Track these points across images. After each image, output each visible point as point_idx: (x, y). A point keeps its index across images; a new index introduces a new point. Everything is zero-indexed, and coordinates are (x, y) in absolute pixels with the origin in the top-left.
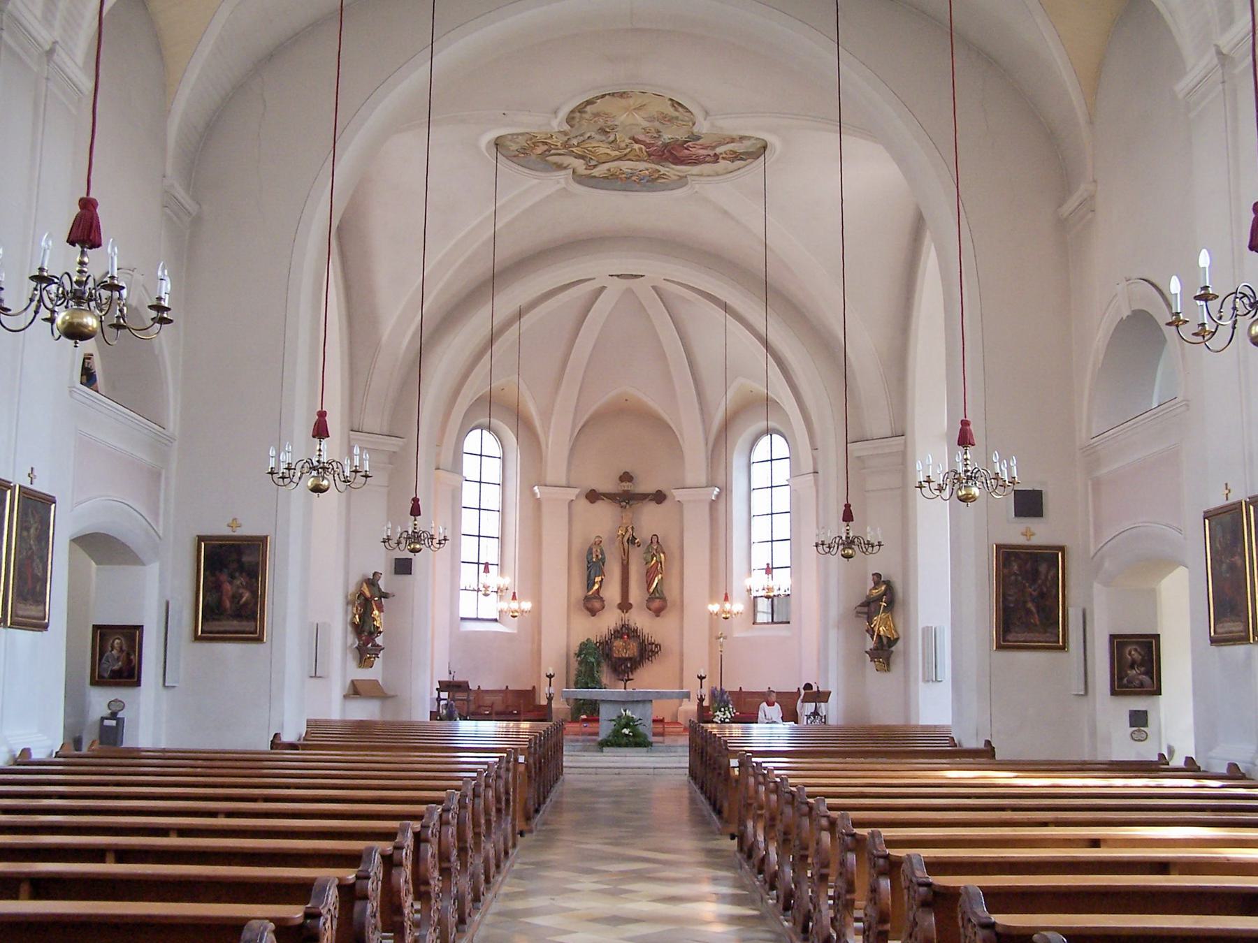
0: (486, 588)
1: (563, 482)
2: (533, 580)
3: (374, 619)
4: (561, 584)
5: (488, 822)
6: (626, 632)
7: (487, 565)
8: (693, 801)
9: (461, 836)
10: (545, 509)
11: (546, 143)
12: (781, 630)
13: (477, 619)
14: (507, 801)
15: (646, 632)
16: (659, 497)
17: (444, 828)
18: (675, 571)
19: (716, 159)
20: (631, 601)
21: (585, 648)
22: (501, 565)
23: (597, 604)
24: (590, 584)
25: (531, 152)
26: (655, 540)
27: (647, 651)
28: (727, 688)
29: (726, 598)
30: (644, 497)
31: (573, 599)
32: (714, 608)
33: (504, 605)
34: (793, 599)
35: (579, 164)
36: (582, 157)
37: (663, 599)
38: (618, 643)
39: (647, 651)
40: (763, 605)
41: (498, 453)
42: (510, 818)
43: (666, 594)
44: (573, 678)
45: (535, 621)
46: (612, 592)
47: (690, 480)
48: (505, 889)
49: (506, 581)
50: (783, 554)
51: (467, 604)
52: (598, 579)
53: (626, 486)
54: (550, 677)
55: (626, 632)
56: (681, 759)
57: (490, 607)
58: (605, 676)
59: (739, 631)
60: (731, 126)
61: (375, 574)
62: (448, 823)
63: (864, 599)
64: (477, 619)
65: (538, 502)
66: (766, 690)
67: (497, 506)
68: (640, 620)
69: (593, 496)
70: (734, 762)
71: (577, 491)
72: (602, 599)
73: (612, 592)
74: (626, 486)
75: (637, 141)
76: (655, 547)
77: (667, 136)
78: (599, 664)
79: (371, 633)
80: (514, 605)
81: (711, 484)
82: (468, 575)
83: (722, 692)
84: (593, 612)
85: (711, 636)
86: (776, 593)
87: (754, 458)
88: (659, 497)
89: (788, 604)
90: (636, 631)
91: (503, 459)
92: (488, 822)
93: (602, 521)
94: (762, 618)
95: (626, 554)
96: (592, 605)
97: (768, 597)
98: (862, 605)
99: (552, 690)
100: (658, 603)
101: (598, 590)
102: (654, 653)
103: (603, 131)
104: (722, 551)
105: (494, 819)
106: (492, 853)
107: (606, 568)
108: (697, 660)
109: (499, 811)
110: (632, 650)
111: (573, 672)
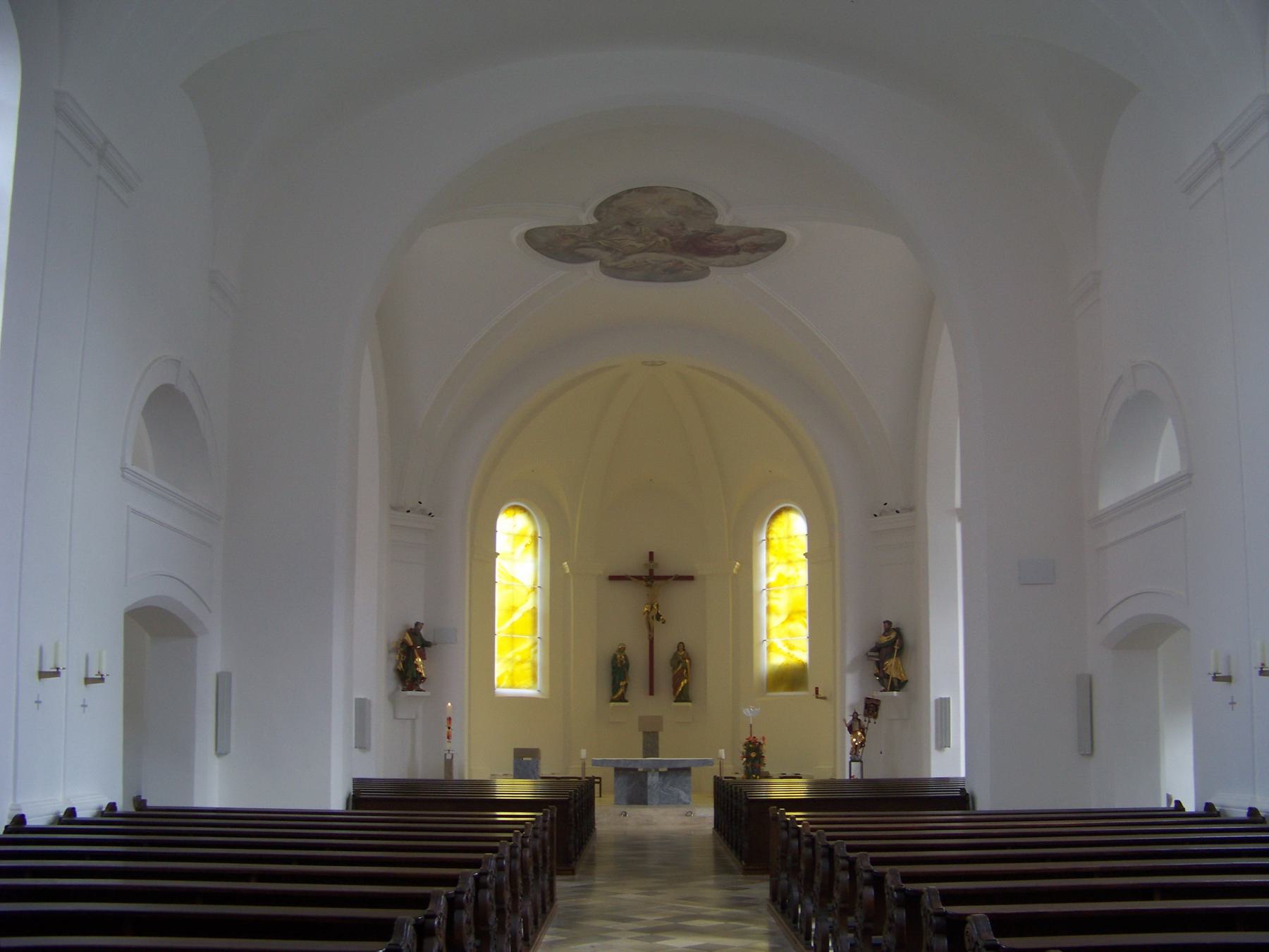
3: (416, 666)
5: (525, 882)
8: (717, 853)
9: (499, 899)
11: (573, 237)
14: (544, 859)
17: (481, 891)
19: (737, 250)
25: (556, 245)
35: (606, 255)
36: (608, 249)
42: (547, 876)
48: (547, 938)
56: (705, 813)
60: (754, 219)
61: (417, 624)
62: (485, 886)
63: (873, 646)
70: (1165, 461)
75: (661, 233)
77: (690, 230)
79: (414, 679)
92: (525, 882)
98: (872, 650)
103: (629, 224)
105: (531, 877)
106: (529, 912)
109: (536, 870)
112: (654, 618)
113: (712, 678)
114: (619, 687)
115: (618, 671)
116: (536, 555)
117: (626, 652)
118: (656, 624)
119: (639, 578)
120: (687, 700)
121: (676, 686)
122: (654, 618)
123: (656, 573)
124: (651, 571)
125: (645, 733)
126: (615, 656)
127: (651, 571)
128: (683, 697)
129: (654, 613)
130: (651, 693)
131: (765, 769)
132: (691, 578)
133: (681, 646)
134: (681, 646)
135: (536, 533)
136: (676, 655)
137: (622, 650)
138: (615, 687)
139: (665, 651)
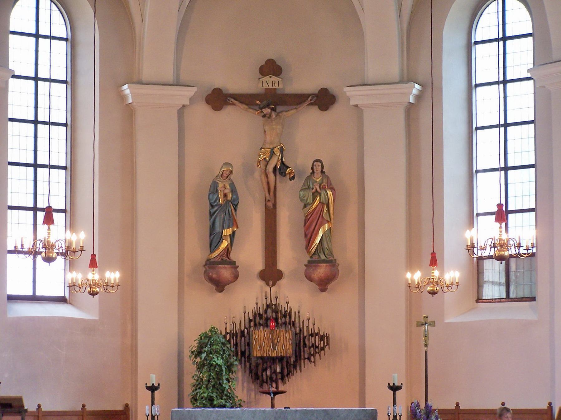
0: (48, 246)
1: (169, 76)
2: (122, 235)
4: (166, 241)
6: (272, 317)
7: (49, 212)
10: (140, 120)
12: (521, 312)
13: (34, 298)
15: (305, 315)
16: (324, 100)
18: (352, 212)
20: (281, 266)
21: (206, 343)
22: (70, 212)
23: (225, 273)
24: (214, 239)
26: (318, 168)
27: (307, 347)
28: (437, 403)
29: (434, 262)
30: (299, 100)
31: (188, 267)
32: (417, 276)
33: (77, 276)
34: (541, 262)
37: (332, 263)
38: (260, 335)
39: (307, 347)
40: (493, 271)
41: (60, 30)
43: (337, 255)
44: (188, 391)
45: (125, 301)
46: (249, 253)
47: (373, 71)
49: (79, 237)
50: (523, 189)
51: (19, 276)
52: (227, 232)
53: (270, 82)
54: (153, 389)
55: (272, 317)
57: (53, 278)
58: (239, 385)
59: (454, 313)
64: (34, 298)
65: (129, 112)
66: (497, 406)
67: (60, 116)
68: (295, 296)
69: (218, 99)
71: (190, 92)
72: (233, 264)
73: (249, 253)
74: (270, 82)
76: (319, 182)
78: (230, 368)
80: (93, 276)
81: (407, 78)
82: (20, 229)
83: (429, 411)
84: (220, 285)
85: (409, 321)
86: (513, 251)
87: (479, 35)
88: (324, 100)
89: (533, 269)
90: (287, 314)
91: (71, 41)
93: (235, 137)
94: (492, 291)
95: (272, 193)
96: (218, 273)
97: (500, 258)
99: (156, 410)
100: (323, 269)
101: (227, 251)
102: (318, 349)
104: (426, 227)
107: (240, 215)
108: (388, 361)
110: (284, 345)
111: (189, 381)
114: (221, 239)
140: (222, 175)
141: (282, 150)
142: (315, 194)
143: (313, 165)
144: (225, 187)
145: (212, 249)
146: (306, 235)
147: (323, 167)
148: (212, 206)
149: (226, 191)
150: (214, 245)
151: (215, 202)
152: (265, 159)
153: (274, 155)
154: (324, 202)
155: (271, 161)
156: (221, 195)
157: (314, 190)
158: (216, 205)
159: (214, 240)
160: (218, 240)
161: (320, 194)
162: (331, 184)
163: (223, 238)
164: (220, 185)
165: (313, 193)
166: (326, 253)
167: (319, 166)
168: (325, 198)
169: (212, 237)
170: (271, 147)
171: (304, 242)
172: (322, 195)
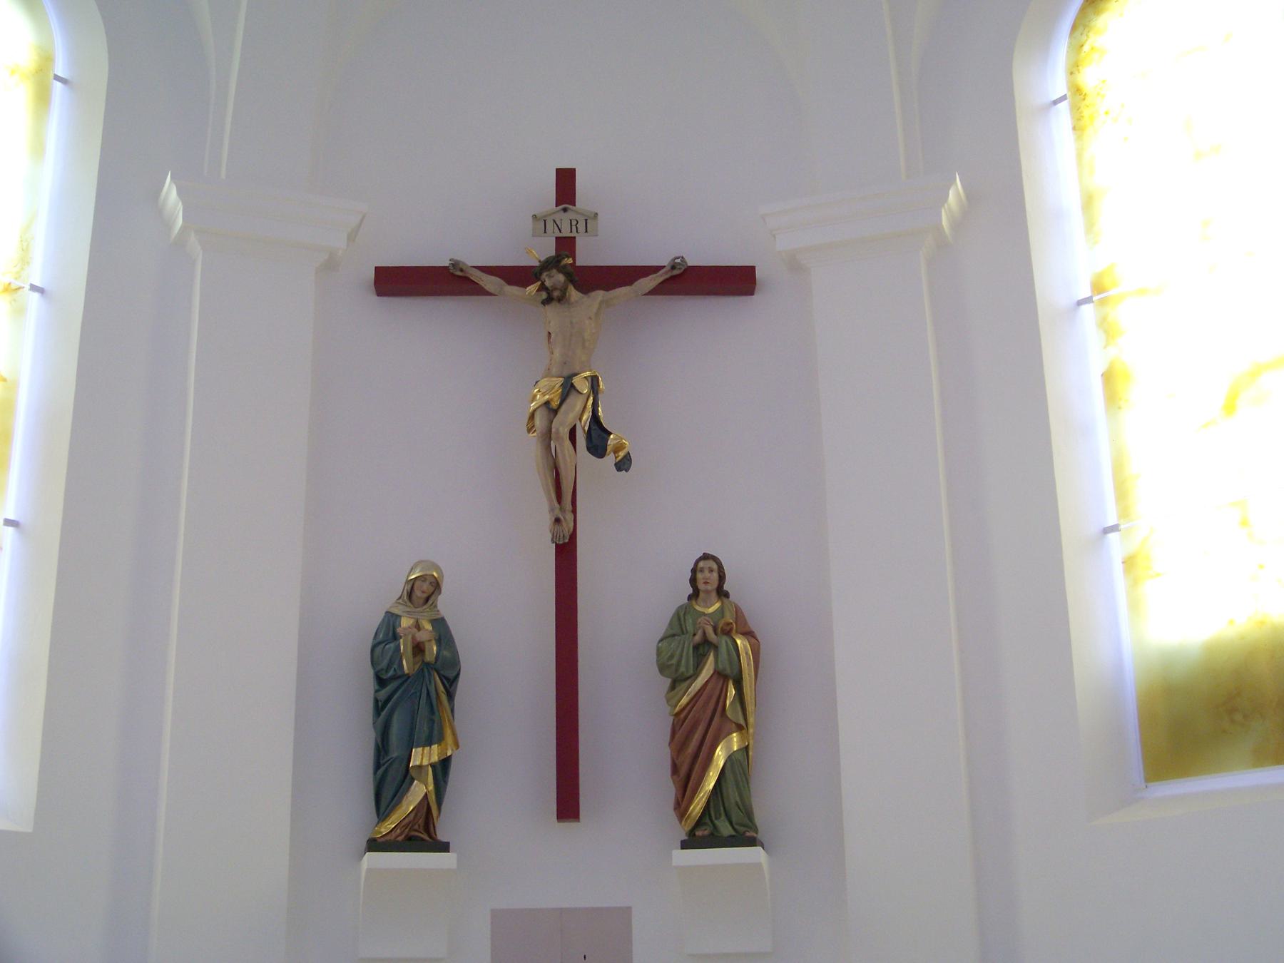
112: (577, 437)
113: (866, 728)
114: (407, 777)
115: (411, 686)
116: (39, 149)
117: (445, 604)
118: (593, 474)
119: (517, 276)
120: (744, 837)
121: (686, 776)
122: (577, 437)
123: (588, 254)
124: (566, 245)
125: (557, 546)
126: (391, 621)
127: (566, 245)
128: (722, 820)
129: (576, 413)
130: (568, 806)
131: (442, 836)
132: (736, 281)
133: (708, 577)
134: (708, 577)
135: (46, 60)
136: (680, 620)
137: (423, 591)
138: (389, 779)
139: (630, 605)
140: (410, 595)
141: (594, 382)
142: (703, 648)
143: (694, 571)
144: (418, 627)
145: (382, 810)
146: (675, 769)
147: (722, 578)
148: (381, 682)
149: (422, 636)
150: (387, 794)
151: (387, 670)
152: (547, 403)
153: (573, 393)
154: (728, 671)
155: (564, 407)
156: (404, 646)
157: (698, 638)
158: (394, 678)
159: (389, 779)
160: (399, 778)
161: (716, 648)
162: (746, 623)
163: (413, 773)
164: (406, 622)
165: (696, 647)
166: (734, 820)
167: (711, 571)
168: (728, 651)
169: (380, 772)
170: (566, 373)
171: (668, 789)
172: (723, 649)
